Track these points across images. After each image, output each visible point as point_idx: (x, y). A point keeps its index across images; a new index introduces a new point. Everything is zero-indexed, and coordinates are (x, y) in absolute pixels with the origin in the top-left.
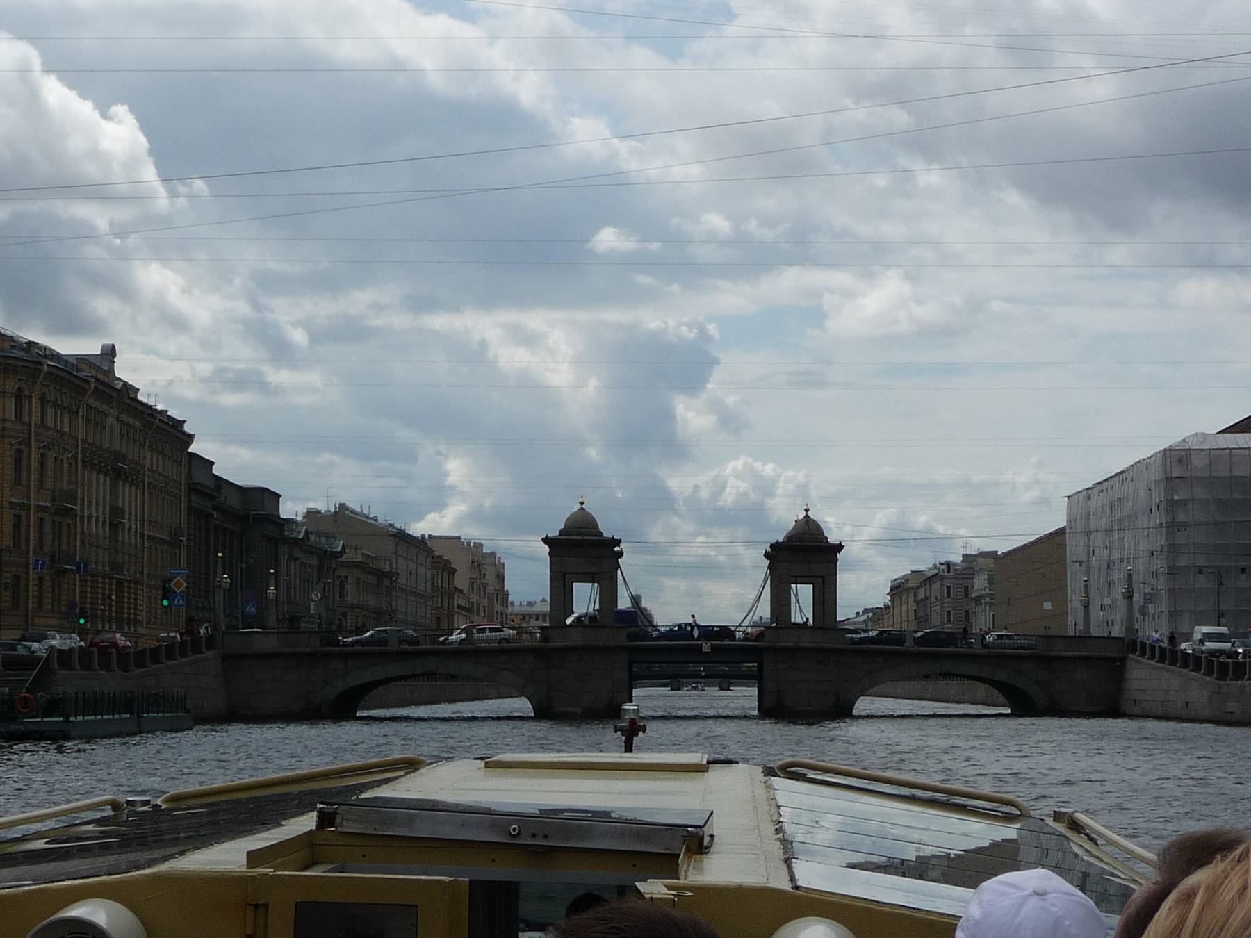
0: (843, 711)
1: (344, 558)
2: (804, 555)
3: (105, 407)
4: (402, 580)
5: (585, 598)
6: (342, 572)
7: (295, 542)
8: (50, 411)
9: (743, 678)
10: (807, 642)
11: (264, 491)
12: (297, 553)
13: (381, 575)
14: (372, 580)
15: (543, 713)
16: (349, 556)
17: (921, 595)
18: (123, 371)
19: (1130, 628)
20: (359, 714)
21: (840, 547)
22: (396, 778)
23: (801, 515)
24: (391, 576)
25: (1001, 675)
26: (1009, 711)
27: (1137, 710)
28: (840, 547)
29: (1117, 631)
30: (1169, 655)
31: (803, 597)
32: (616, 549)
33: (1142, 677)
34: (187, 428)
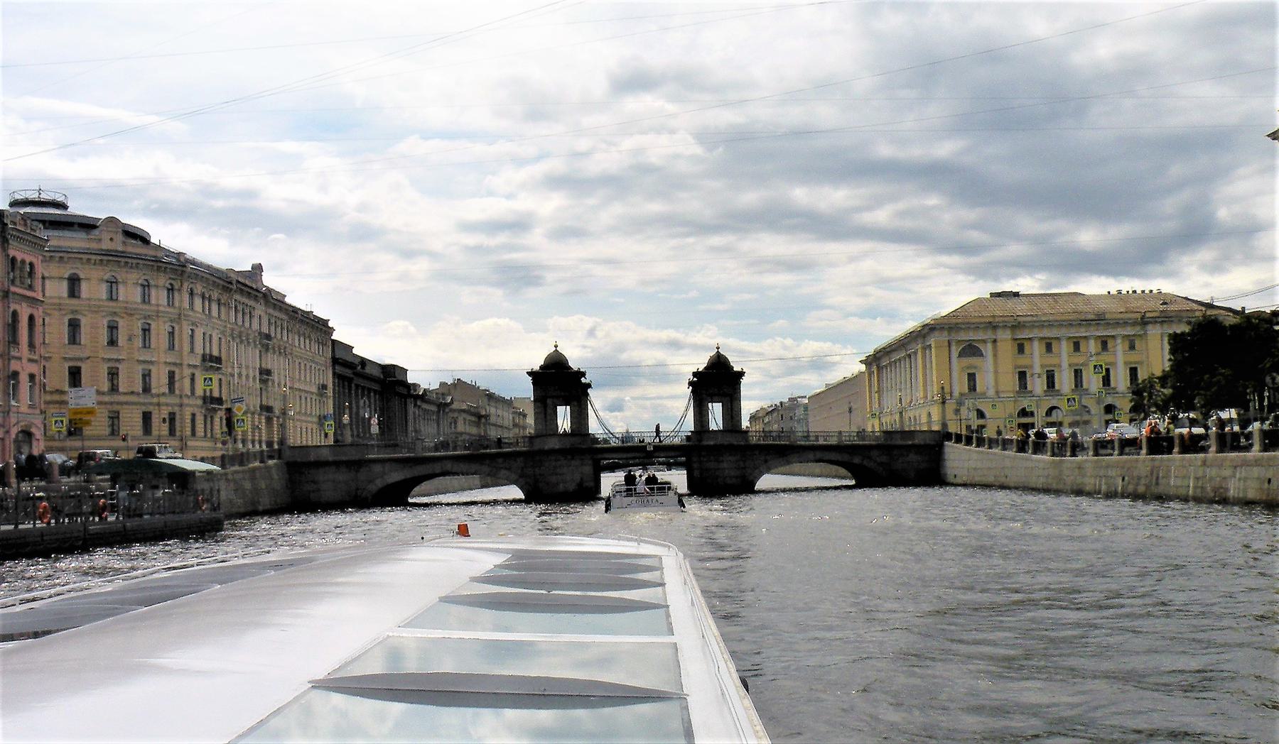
0: (746, 487)
1: (454, 406)
2: (717, 381)
3: (251, 303)
4: (493, 419)
5: (564, 418)
6: (456, 415)
7: (417, 397)
8: (198, 302)
9: (678, 465)
10: (720, 440)
11: (394, 366)
12: (419, 403)
13: (480, 417)
14: (473, 419)
15: (533, 496)
16: (454, 406)
17: (766, 420)
18: (270, 280)
19: (944, 425)
20: (410, 500)
21: (741, 374)
22: (192, 586)
23: (713, 353)
24: (487, 417)
25: (857, 460)
26: (853, 482)
27: (958, 481)
28: (741, 374)
29: (936, 428)
30: (973, 437)
31: (716, 413)
32: (583, 380)
33: (957, 458)
34: (330, 325)
